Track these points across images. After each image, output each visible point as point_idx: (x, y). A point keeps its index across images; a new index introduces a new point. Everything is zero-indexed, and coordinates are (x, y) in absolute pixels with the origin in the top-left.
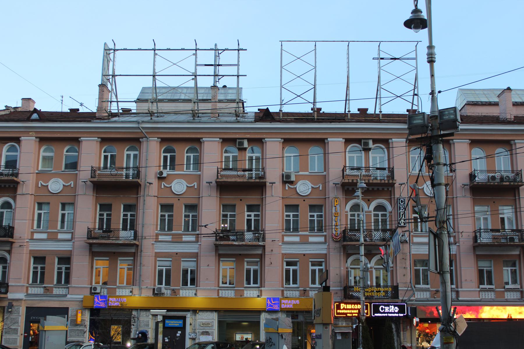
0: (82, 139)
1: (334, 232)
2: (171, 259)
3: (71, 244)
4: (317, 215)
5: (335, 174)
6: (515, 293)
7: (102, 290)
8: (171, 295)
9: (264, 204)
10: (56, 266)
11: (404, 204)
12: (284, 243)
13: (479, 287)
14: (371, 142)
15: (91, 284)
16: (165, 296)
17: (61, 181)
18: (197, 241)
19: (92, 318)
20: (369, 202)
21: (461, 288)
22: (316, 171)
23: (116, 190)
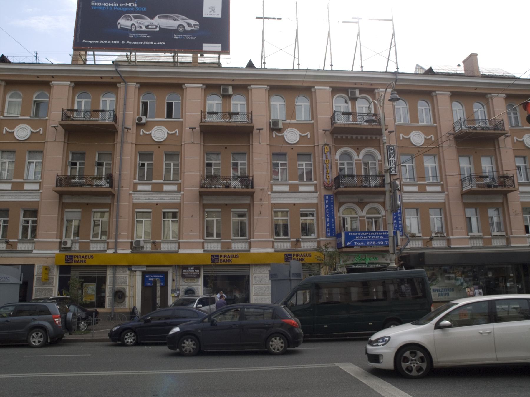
0: (53, 82)
1: (326, 180)
2: (150, 210)
3: (39, 194)
4: (306, 164)
5: (323, 122)
6: (501, 240)
7: (74, 244)
8: (152, 248)
9: (251, 151)
10: (22, 219)
11: (394, 152)
12: (273, 192)
13: (468, 235)
14: (357, 92)
15: (61, 238)
16: (145, 249)
17: (29, 127)
18: (179, 191)
19: (61, 275)
20: (358, 150)
21: (453, 235)
22: (303, 119)
23: (87, 135)
